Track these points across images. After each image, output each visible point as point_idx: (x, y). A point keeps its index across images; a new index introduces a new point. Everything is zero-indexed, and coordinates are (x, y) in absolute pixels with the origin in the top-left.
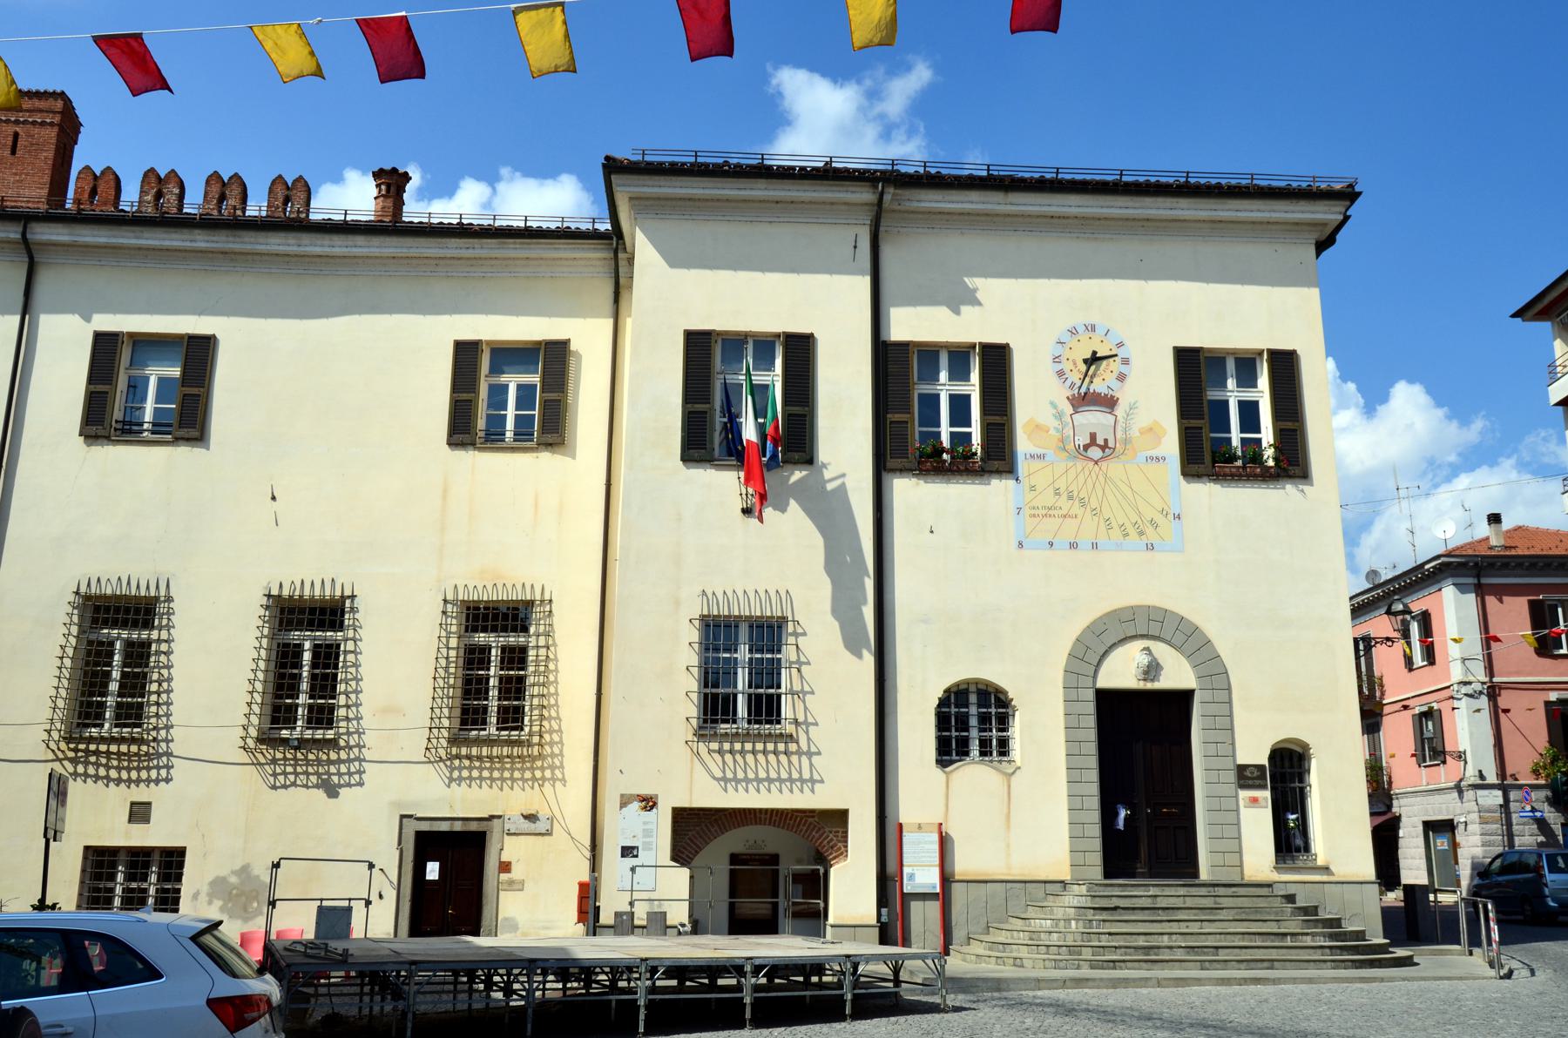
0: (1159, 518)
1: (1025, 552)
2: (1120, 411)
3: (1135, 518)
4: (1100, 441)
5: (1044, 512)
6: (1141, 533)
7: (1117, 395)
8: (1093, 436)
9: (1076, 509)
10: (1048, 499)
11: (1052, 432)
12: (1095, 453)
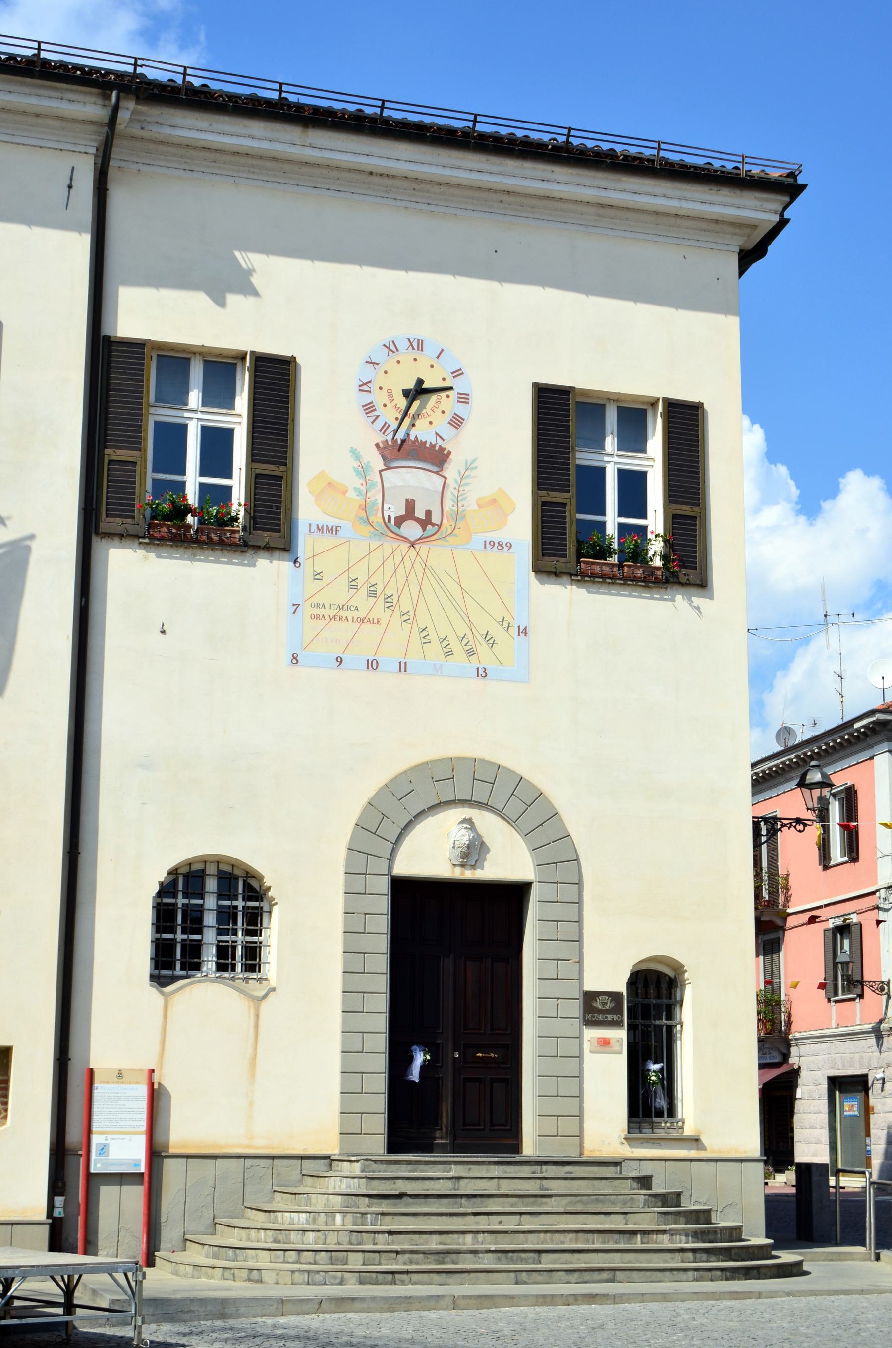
0: (497, 632)
1: (300, 670)
2: (452, 470)
3: (463, 630)
4: (420, 514)
5: (333, 612)
6: (471, 652)
7: (448, 447)
8: (410, 506)
9: (379, 611)
10: (339, 593)
11: (352, 494)
12: (411, 529)
